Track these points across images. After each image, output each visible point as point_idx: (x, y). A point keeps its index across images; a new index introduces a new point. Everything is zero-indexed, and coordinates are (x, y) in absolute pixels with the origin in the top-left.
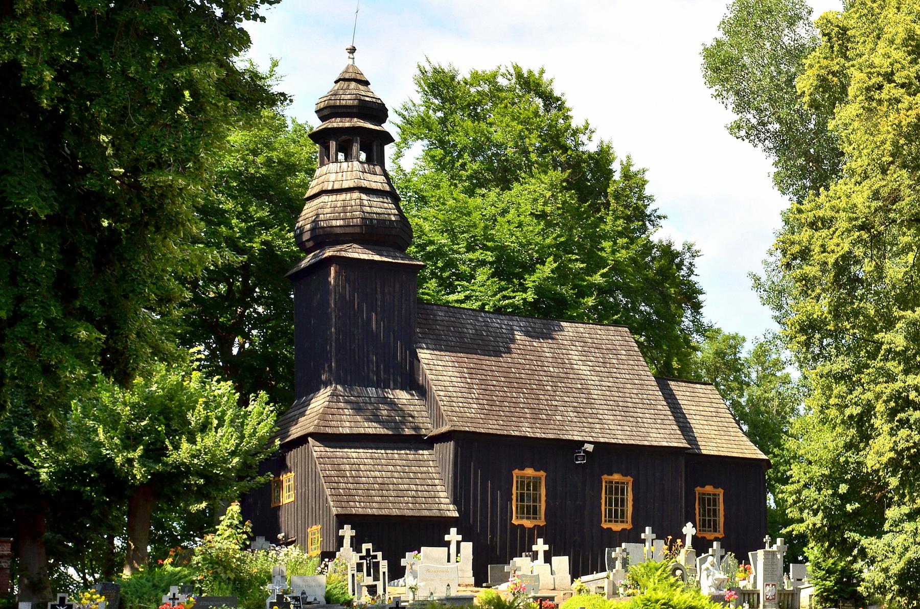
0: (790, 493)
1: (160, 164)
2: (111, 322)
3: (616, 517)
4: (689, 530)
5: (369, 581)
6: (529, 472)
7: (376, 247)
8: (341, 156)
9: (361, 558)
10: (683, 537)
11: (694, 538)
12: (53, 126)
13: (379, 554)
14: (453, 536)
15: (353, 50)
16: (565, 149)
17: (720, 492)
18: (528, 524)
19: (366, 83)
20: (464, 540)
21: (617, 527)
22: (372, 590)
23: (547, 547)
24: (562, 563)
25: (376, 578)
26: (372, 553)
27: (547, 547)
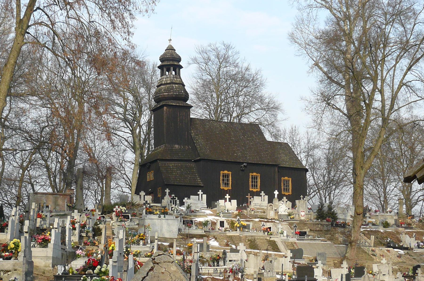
0: (162, 75)
4: (276, 193)
6: (226, 172)
7: (187, 105)
9: (171, 199)
13: (177, 198)
14: (200, 192)
15: (170, 40)
19: (175, 50)
20: (146, 195)
21: (255, 190)
23: (229, 197)
24: (234, 202)
27: (229, 197)
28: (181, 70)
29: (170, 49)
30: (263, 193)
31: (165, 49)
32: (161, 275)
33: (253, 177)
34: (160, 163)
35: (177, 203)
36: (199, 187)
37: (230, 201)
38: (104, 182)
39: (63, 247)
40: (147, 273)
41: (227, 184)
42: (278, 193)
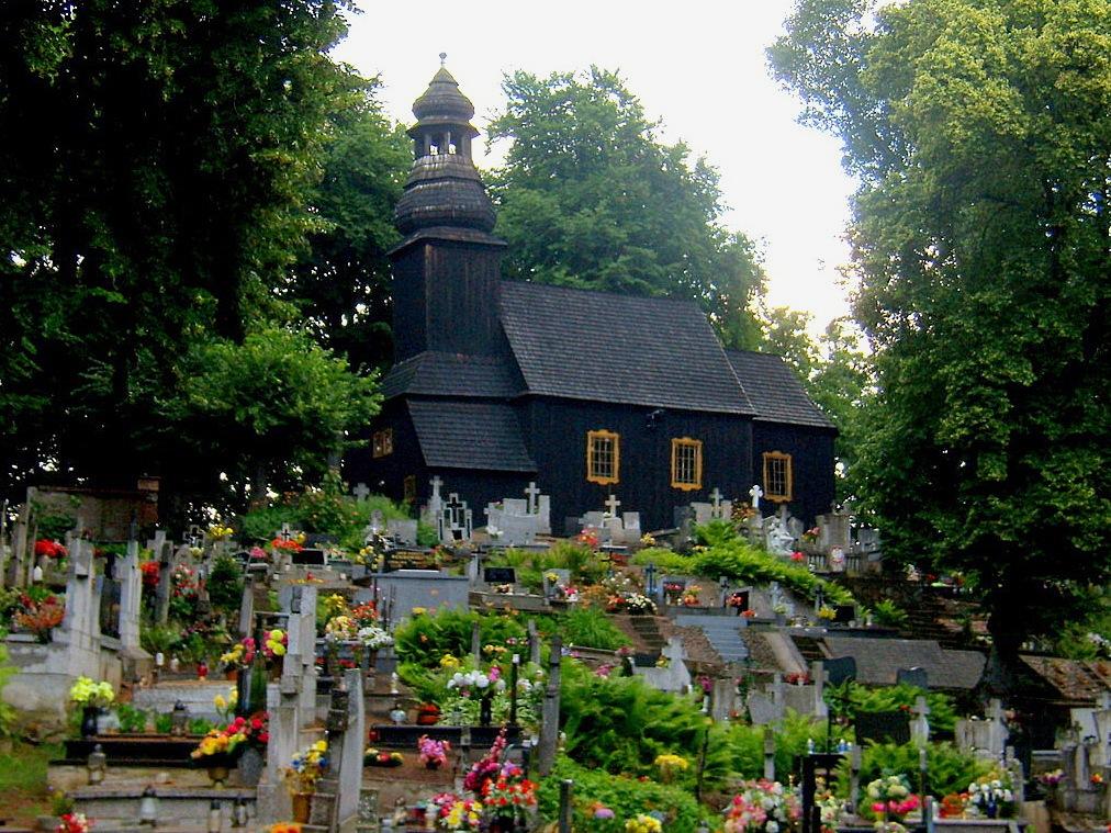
1: (268, 143)
3: (686, 477)
4: (756, 492)
5: (455, 527)
6: (603, 433)
11: (761, 500)
13: (464, 503)
14: (532, 489)
15: (443, 56)
16: (640, 141)
17: (789, 457)
18: (603, 481)
21: (687, 487)
22: (457, 535)
23: (618, 503)
25: (462, 525)
26: (457, 502)
27: (618, 503)
28: (473, 141)
29: (443, 82)
30: (717, 496)
31: (431, 80)
33: (681, 450)
34: (411, 405)
35: (466, 518)
36: (526, 478)
37: (619, 514)
39: (111, 642)
41: (608, 470)
42: (441, 483)
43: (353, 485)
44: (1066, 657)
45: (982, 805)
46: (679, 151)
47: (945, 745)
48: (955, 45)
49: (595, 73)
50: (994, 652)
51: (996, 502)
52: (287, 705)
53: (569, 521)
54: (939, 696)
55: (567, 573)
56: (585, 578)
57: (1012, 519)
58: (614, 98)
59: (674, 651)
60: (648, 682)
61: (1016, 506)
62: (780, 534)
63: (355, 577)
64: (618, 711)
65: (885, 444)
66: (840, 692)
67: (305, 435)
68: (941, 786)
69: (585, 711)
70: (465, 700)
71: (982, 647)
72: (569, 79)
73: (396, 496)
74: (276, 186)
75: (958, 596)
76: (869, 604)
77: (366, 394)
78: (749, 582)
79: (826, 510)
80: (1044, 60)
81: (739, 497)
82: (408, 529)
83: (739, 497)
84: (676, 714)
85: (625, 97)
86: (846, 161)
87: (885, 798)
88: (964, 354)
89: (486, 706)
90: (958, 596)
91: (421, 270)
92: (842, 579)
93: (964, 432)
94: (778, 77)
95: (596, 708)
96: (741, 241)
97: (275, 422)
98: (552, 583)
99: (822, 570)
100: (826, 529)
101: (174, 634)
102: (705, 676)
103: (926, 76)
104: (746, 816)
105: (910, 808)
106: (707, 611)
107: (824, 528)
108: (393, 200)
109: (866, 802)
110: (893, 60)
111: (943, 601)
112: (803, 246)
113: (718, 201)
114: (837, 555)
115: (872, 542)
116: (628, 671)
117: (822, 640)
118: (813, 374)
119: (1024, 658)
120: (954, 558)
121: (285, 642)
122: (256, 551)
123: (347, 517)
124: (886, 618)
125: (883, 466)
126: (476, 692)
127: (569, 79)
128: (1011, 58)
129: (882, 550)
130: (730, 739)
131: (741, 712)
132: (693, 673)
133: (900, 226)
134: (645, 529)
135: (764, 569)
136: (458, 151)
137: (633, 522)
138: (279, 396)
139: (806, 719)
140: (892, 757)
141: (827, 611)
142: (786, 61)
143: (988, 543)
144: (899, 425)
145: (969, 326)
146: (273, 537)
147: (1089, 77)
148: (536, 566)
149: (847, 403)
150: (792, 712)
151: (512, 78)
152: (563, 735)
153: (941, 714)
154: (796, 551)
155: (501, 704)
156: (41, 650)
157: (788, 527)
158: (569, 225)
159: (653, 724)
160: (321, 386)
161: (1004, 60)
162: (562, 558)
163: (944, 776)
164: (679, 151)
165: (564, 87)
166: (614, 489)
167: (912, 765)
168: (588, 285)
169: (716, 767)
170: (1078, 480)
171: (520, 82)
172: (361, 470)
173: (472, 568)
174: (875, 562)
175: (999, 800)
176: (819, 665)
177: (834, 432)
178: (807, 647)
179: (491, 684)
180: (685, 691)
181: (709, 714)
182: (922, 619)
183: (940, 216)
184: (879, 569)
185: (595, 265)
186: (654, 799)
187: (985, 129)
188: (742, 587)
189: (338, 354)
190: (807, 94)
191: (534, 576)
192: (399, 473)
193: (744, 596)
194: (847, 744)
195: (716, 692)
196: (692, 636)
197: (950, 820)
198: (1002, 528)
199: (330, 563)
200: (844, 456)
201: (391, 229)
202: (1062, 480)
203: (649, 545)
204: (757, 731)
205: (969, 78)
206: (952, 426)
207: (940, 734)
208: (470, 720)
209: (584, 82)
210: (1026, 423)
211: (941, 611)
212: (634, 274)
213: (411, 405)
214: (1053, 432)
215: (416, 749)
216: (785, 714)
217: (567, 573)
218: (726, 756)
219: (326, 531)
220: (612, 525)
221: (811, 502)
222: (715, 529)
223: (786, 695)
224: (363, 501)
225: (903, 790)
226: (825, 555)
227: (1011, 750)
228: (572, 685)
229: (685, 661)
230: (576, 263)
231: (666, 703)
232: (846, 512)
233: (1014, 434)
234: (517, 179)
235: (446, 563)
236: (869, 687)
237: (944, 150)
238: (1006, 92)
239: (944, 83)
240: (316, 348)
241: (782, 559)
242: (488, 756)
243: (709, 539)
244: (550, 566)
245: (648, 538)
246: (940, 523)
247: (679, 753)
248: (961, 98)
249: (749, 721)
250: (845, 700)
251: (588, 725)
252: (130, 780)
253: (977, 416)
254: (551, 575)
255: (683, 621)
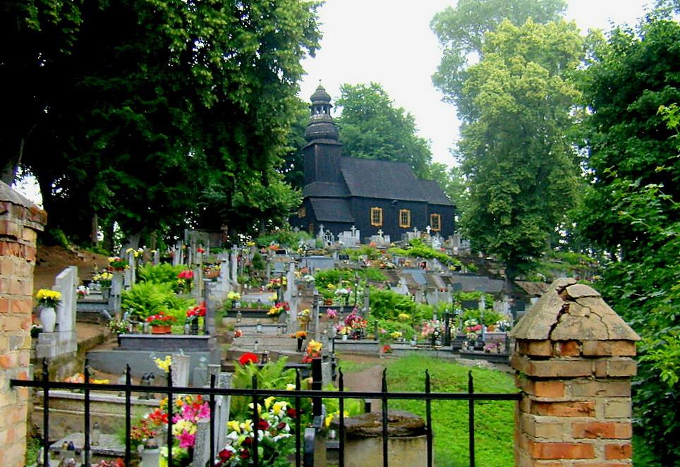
1: (277, 126)
2: (263, 169)
4: (428, 228)
5: (328, 241)
6: (377, 208)
8: (318, 112)
10: (426, 231)
11: (430, 231)
12: (247, 118)
13: (331, 234)
14: (353, 228)
16: (387, 108)
18: (377, 225)
21: (405, 226)
22: (329, 244)
29: (320, 89)
30: (415, 229)
32: (585, 321)
34: (312, 200)
36: (352, 224)
38: (663, 217)
39: (231, 281)
40: (559, 317)
41: (378, 221)
43: (294, 227)
44: (530, 281)
45: (500, 328)
46: (401, 110)
47: (490, 310)
48: (493, 82)
49: (372, 84)
50: (507, 280)
51: (507, 231)
52: (293, 299)
53: (366, 238)
54: (489, 295)
55: (366, 256)
56: (372, 258)
57: (512, 237)
58: (378, 92)
59: (403, 281)
60: (396, 291)
61: (514, 233)
62: (436, 242)
63: (297, 258)
64: (386, 301)
65: (471, 212)
66: (456, 294)
67: (274, 212)
68: (488, 322)
69: (376, 301)
70: (340, 297)
71: (503, 279)
72: (363, 86)
73: (306, 229)
74: (279, 138)
75: (495, 262)
76: (466, 265)
77: (297, 197)
78: (426, 258)
79: (452, 234)
80: (522, 87)
81: (423, 230)
82: (313, 242)
83: (423, 230)
84: (405, 302)
85: (382, 92)
86: (458, 115)
87: (470, 326)
88: (497, 183)
89: (347, 299)
90: (495, 262)
91: (314, 156)
92: (458, 257)
93: (497, 209)
94: (435, 86)
95: (380, 300)
96: (423, 141)
97: (267, 207)
98: (361, 260)
99: (451, 254)
100: (452, 240)
101: (246, 278)
102: (413, 289)
103: (484, 92)
104: (428, 330)
105: (477, 329)
106: (413, 268)
107: (451, 240)
108: (304, 130)
109: (465, 328)
110: (473, 85)
111: (490, 263)
112: (441, 135)
113: (415, 127)
114: (456, 249)
115: (467, 243)
116: (389, 289)
117: (450, 277)
118: (447, 186)
119: (516, 282)
120: (494, 250)
121: (286, 281)
122: (263, 250)
123: (292, 238)
124: (472, 270)
125: (471, 220)
126: (344, 295)
127: (363, 86)
128: (512, 86)
129: (471, 247)
130: (422, 309)
131: (425, 301)
132: (409, 289)
133: (475, 141)
134: (391, 241)
135: (431, 254)
136: (326, 113)
137: (388, 239)
138: (269, 198)
139: (447, 303)
140: (472, 314)
141: (452, 268)
142: (438, 81)
143: (505, 245)
144: (476, 206)
145: (498, 174)
146: (268, 246)
147: (537, 93)
148: (356, 254)
149: (459, 196)
150: (441, 301)
151: (343, 86)
152: (370, 308)
153: (489, 301)
154: (442, 247)
155: (351, 299)
156: (214, 283)
157: (440, 240)
158: (364, 136)
159: (398, 304)
160: (282, 195)
161: (509, 87)
162: (364, 251)
163: (489, 319)
164: (401, 110)
165: (361, 89)
166: (380, 227)
167: (479, 316)
168: (370, 157)
169: (417, 317)
170: (534, 224)
171: (346, 88)
172: (294, 222)
173: (335, 255)
174: (468, 251)
175: (506, 326)
176: (449, 285)
177: (455, 207)
178: (446, 280)
179: (349, 293)
180: (407, 294)
181: (414, 301)
182: (483, 270)
183: (489, 136)
184: (469, 253)
185: (373, 150)
186: (399, 327)
187: (503, 109)
188: (424, 260)
189: (288, 183)
190: (444, 91)
191: (355, 257)
192: (308, 222)
193: (425, 263)
194: (458, 311)
195: (416, 294)
196: (408, 277)
197: (490, 333)
198: (509, 240)
199: (288, 254)
200: (458, 214)
201: (303, 139)
202: (529, 224)
203: (393, 247)
204: (430, 306)
205: (498, 93)
206: (493, 207)
207: (489, 307)
208: (342, 304)
209: (367, 87)
210: (518, 205)
211: (489, 267)
212: (386, 153)
213: (312, 200)
214: (526, 208)
215: (326, 313)
216: (439, 301)
217: (366, 256)
218: (421, 314)
219: (560, 357)
220: (380, 240)
221: (447, 231)
222: (415, 240)
223: (439, 296)
224: (296, 233)
225: (475, 323)
226: (452, 249)
227: (510, 311)
228: (372, 293)
229: (407, 285)
230: (366, 150)
231: (402, 298)
232: (458, 234)
233: (513, 209)
234: (345, 121)
235: (326, 254)
236: (466, 292)
237: (489, 117)
238: (510, 98)
239: (490, 95)
240: (280, 182)
241: (437, 251)
242: (352, 314)
243: (413, 244)
244: (361, 254)
245: (393, 244)
246: (489, 238)
247: (406, 313)
248: (495, 100)
249: (427, 304)
250: (458, 297)
251: (377, 305)
252: (249, 321)
253: (501, 204)
254: (361, 257)
255: (405, 271)
